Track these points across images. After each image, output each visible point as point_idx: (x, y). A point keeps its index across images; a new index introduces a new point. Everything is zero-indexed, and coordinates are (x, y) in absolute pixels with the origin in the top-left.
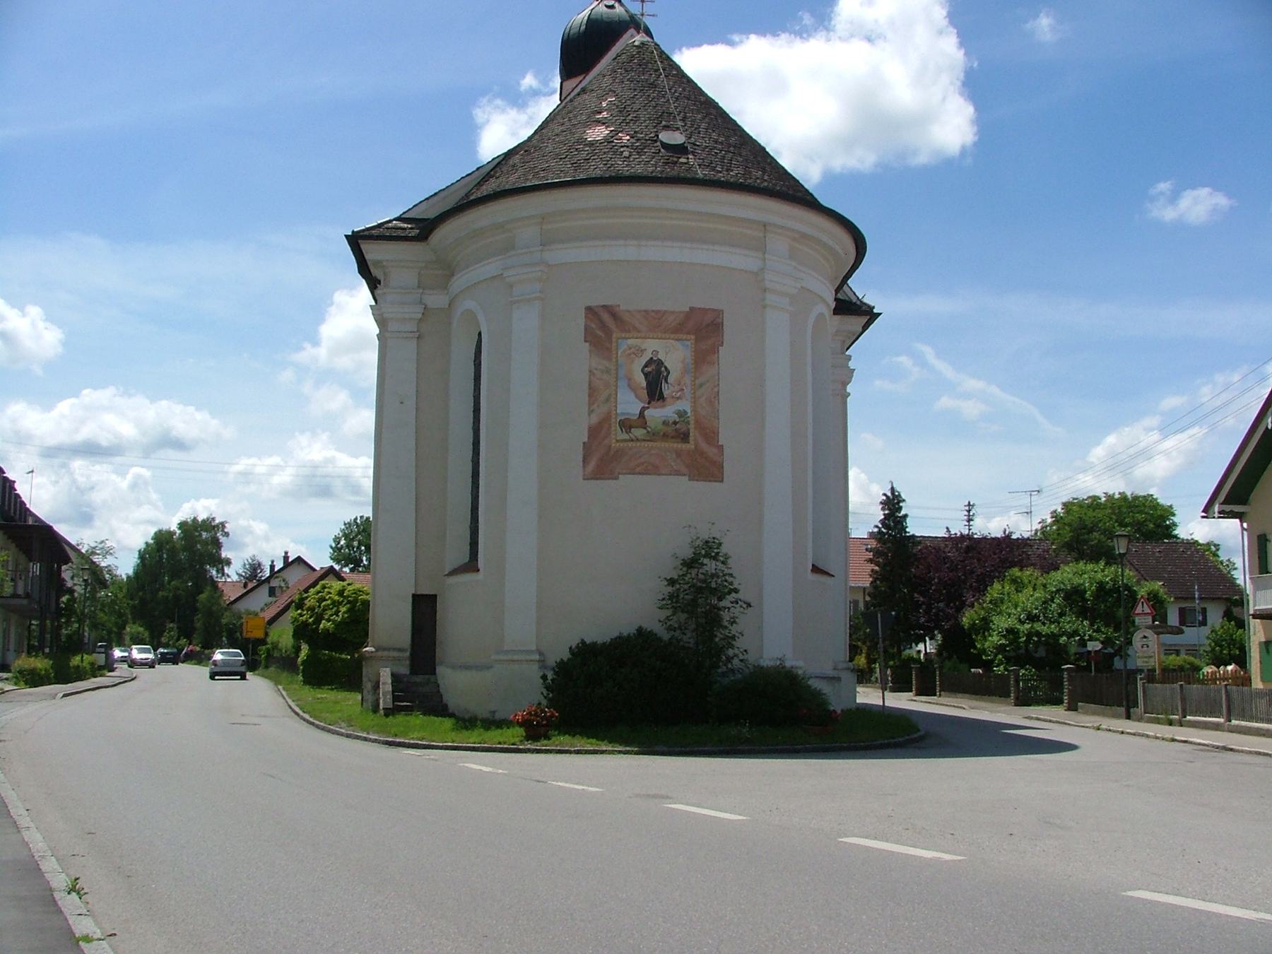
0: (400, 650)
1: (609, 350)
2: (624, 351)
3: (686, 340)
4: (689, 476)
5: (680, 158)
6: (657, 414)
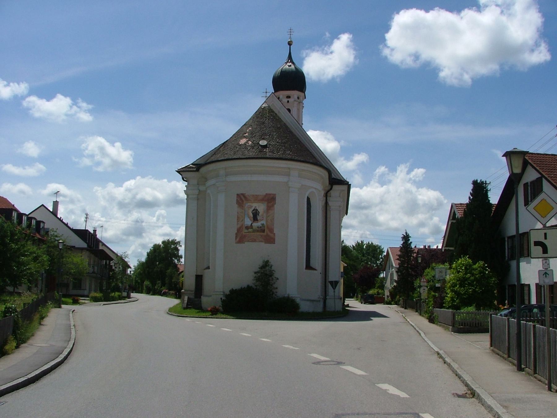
0: (192, 291)
1: (243, 206)
2: (247, 207)
5: (264, 149)
6: (255, 225)
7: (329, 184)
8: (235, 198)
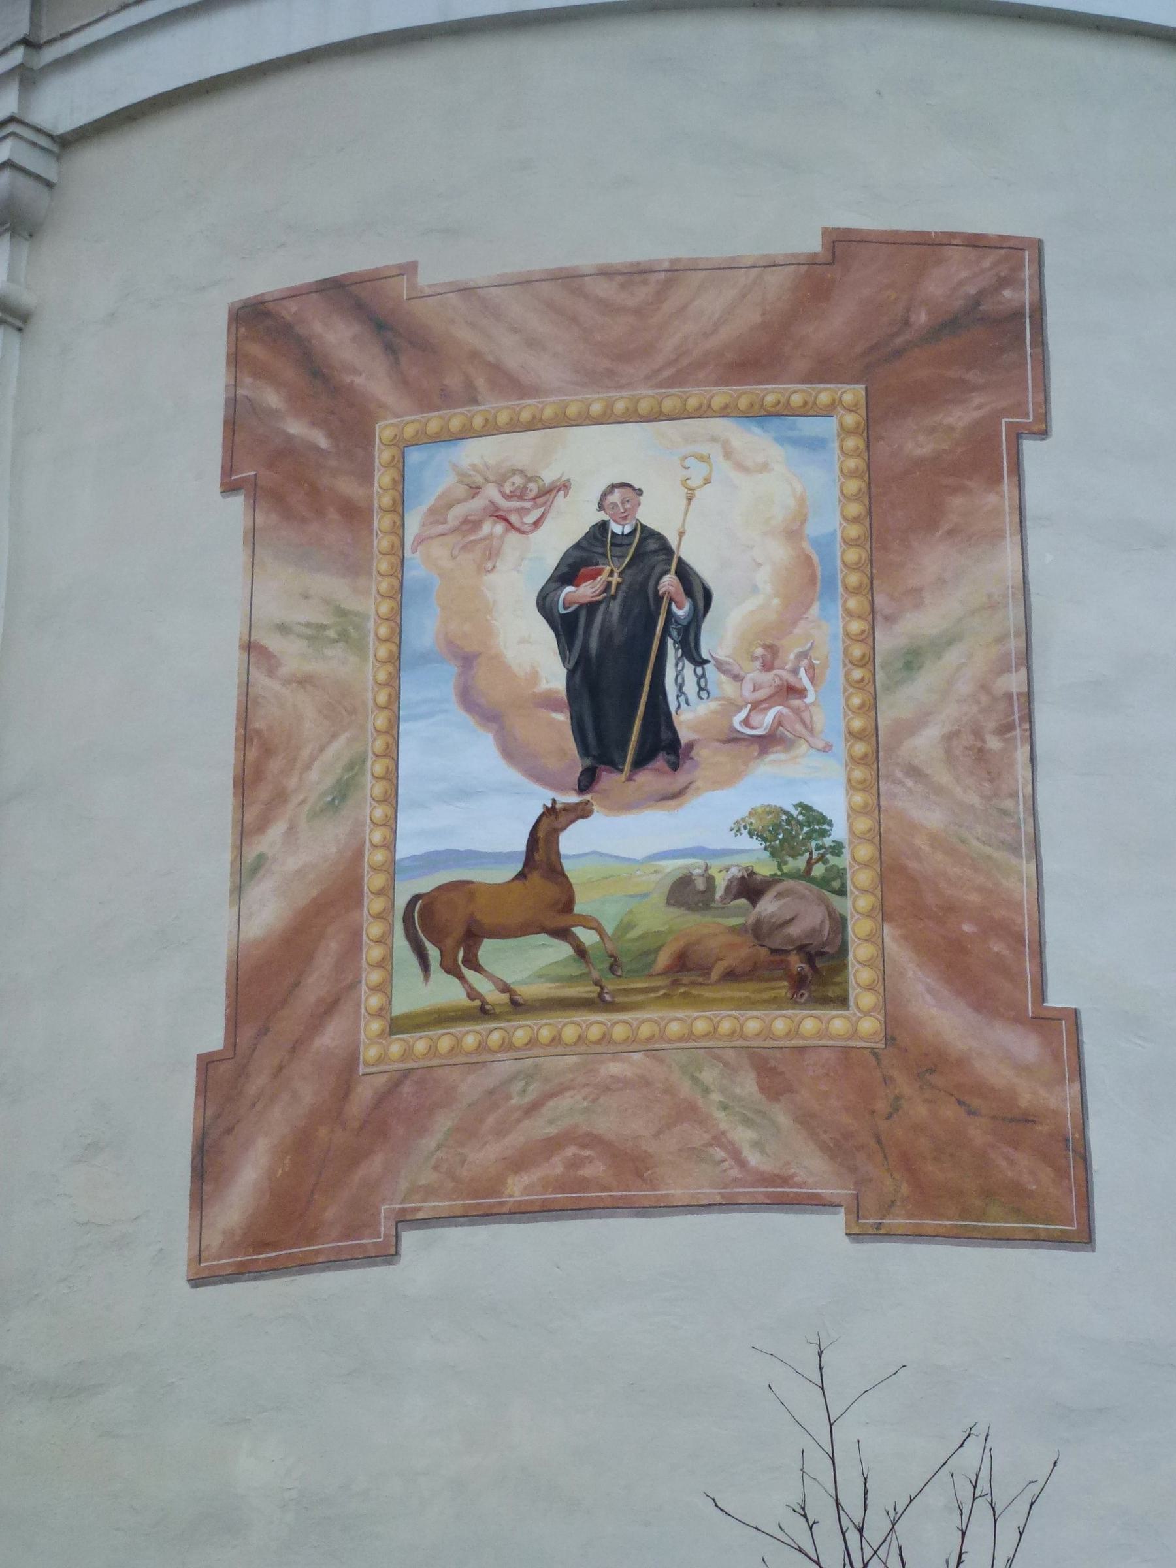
2: (436, 514)
3: (808, 410)
4: (856, 1211)
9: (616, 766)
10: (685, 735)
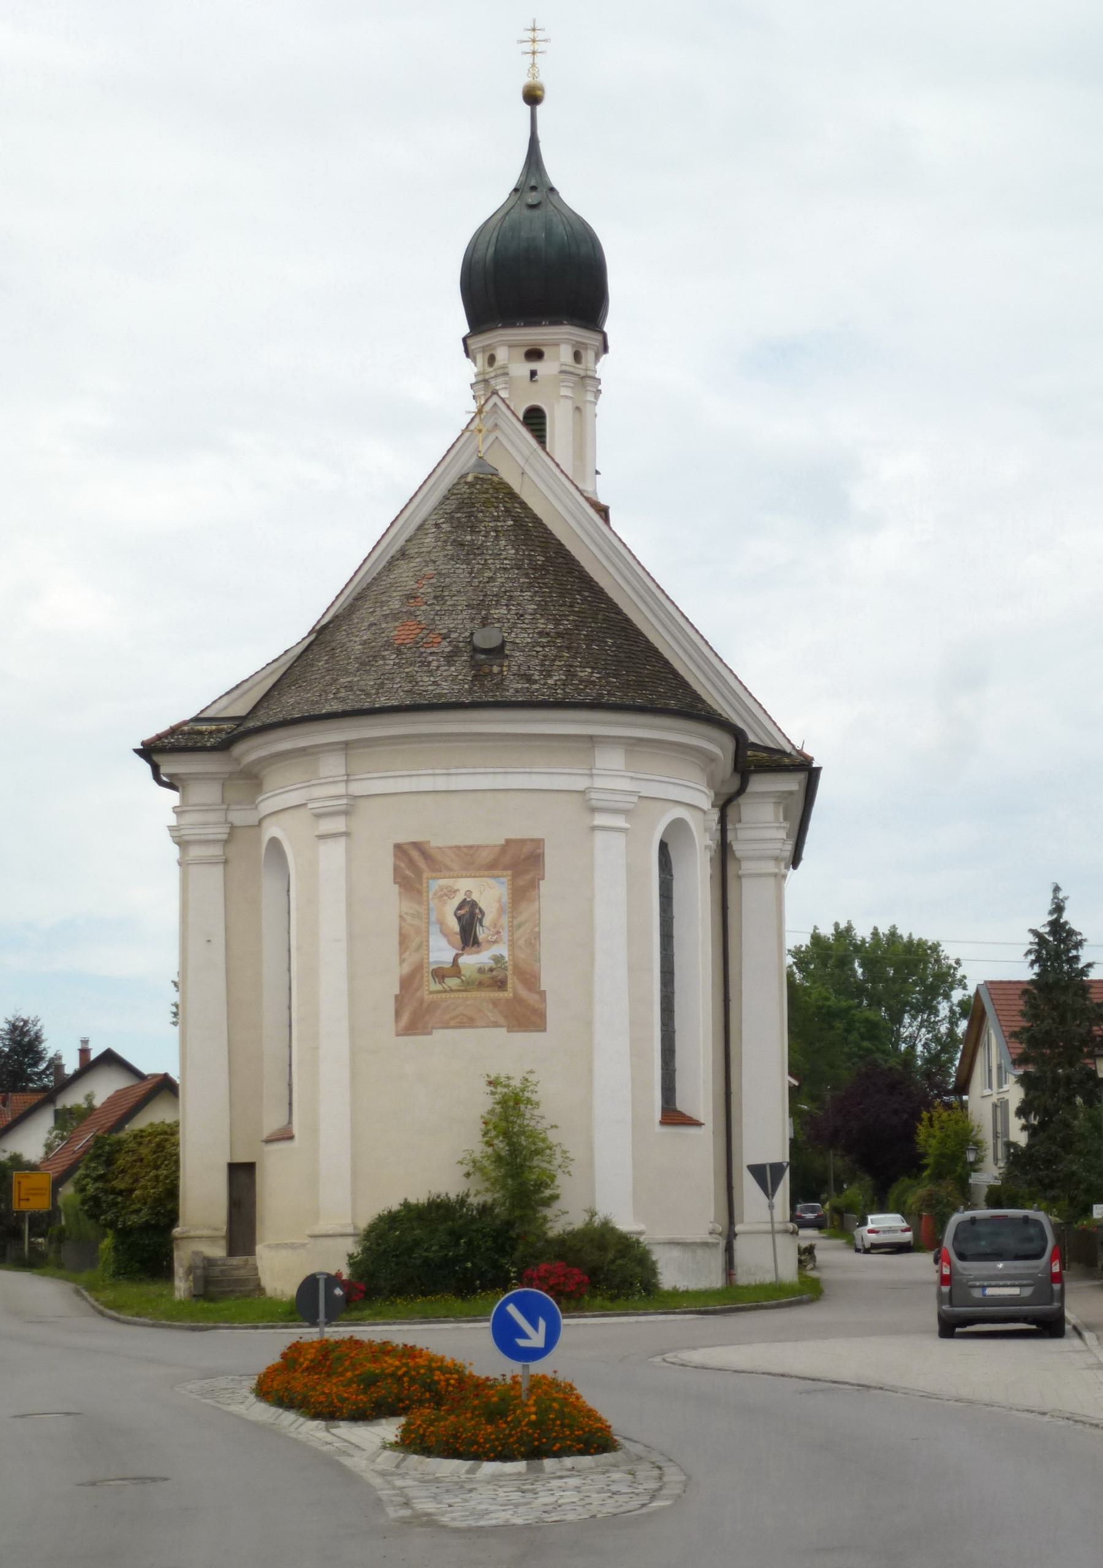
1: (420, 892)
2: (435, 894)
4: (508, 1027)
6: (471, 961)
7: (736, 769)
8: (388, 860)
9: (468, 946)
10: (480, 940)
